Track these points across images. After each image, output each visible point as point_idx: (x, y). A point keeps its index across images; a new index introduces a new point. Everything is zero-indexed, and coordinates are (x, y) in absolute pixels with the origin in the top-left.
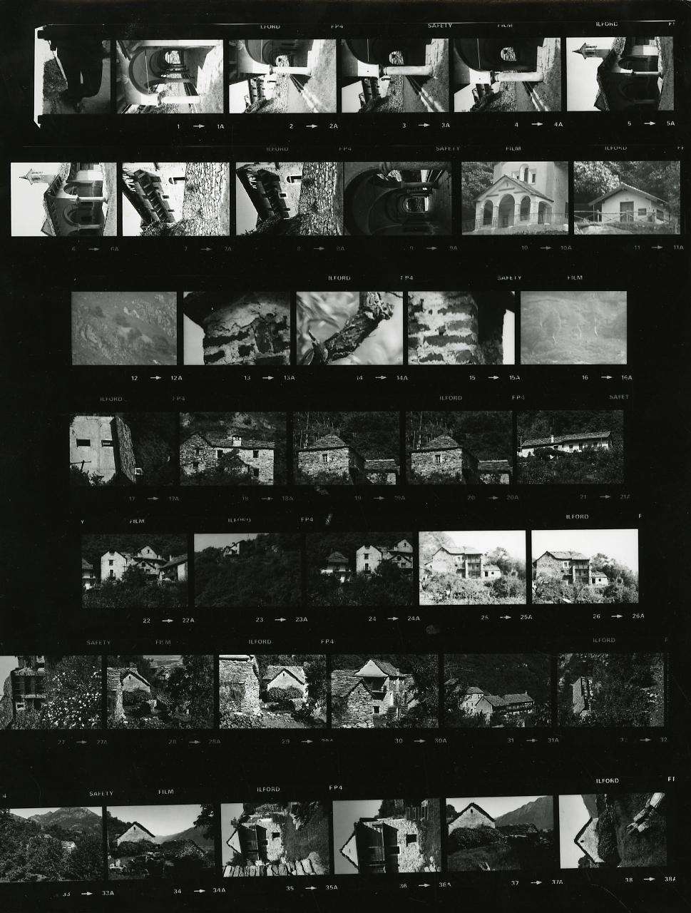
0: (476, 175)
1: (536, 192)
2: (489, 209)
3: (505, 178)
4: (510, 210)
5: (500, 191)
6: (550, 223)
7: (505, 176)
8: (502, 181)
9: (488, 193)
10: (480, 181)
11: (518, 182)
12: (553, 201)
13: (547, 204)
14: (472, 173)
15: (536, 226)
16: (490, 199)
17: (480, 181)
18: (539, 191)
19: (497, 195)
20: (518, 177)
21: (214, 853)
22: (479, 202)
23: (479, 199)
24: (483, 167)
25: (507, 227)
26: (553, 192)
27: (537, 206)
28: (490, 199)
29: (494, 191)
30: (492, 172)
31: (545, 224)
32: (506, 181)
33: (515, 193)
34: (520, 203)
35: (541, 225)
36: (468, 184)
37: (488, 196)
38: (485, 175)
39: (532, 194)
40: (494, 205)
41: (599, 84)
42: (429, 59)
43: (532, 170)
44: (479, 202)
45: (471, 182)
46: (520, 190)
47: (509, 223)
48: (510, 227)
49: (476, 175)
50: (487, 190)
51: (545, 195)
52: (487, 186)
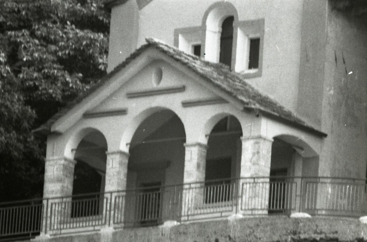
0: (46, 40)
1: (264, 101)
2: (93, 162)
3: (151, 53)
4: (168, 164)
5: (132, 96)
6: (312, 211)
7: (150, 45)
8: (141, 61)
9: (88, 105)
10: (60, 61)
11: (197, 65)
12: (320, 135)
13: (302, 146)
14: (33, 35)
15: (259, 222)
16: (99, 124)
17: (60, 61)
18: (272, 97)
19: (122, 112)
20: (198, 50)
21: (218, 8)
22: (58, 134)
23: (60, 126)
24: (73, 13)
25: (156, 223)
26: (325, 102)
27: (266, 150)
28: (99, 124)
29: (109, 98)
30: (105, 28)
31: (296, 215)
32: (154, 62)
33: (186, 104)
34: (204, 141)
35: (279, 220)
36: (17, 72)
37: (88, 115)
38: (79, 40)
39: (248, 110)
40: (111, 148)
41: (154, 107)
42: (262, 163)
43: (247, 25)
44: (58, 134)
45: (29, 64)
46: (203, 96)
47: (167, 207)
48: (169, 224)
49: (46, 40)
50: (88, 94)
51: (295, 114)
52: (84, 81)
